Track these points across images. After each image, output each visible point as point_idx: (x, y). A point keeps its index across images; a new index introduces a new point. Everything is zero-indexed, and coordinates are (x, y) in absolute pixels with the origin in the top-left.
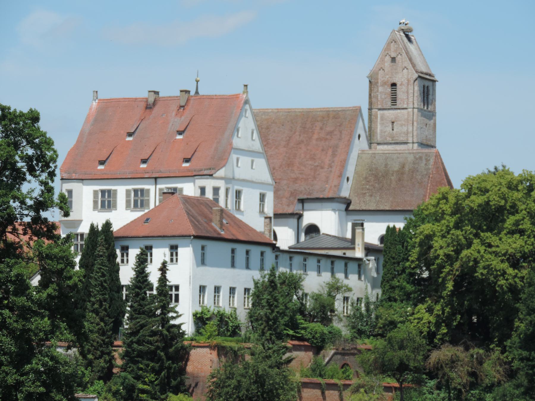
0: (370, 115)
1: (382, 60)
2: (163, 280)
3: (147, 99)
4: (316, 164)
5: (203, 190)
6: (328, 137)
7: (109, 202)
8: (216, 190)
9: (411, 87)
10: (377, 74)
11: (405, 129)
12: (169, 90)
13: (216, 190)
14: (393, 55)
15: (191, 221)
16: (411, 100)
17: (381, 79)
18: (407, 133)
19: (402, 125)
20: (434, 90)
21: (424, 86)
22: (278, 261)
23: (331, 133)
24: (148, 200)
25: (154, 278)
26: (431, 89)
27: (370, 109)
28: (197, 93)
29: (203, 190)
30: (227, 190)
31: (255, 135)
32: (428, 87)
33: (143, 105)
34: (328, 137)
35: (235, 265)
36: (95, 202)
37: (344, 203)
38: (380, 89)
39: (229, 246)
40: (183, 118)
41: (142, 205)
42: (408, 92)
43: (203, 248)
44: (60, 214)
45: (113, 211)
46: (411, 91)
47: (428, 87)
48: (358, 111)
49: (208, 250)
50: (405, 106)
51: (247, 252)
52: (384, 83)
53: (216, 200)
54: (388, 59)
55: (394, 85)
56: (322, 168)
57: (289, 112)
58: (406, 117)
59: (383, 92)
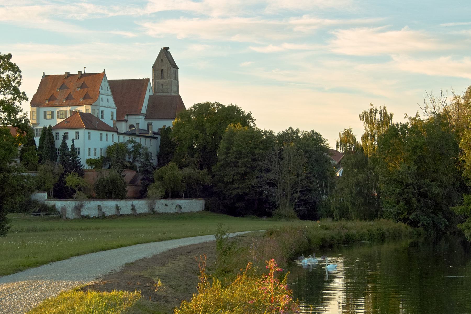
12: (74, 71)
14: (162, 58)
31: (109, 89)
55: (162, 70)
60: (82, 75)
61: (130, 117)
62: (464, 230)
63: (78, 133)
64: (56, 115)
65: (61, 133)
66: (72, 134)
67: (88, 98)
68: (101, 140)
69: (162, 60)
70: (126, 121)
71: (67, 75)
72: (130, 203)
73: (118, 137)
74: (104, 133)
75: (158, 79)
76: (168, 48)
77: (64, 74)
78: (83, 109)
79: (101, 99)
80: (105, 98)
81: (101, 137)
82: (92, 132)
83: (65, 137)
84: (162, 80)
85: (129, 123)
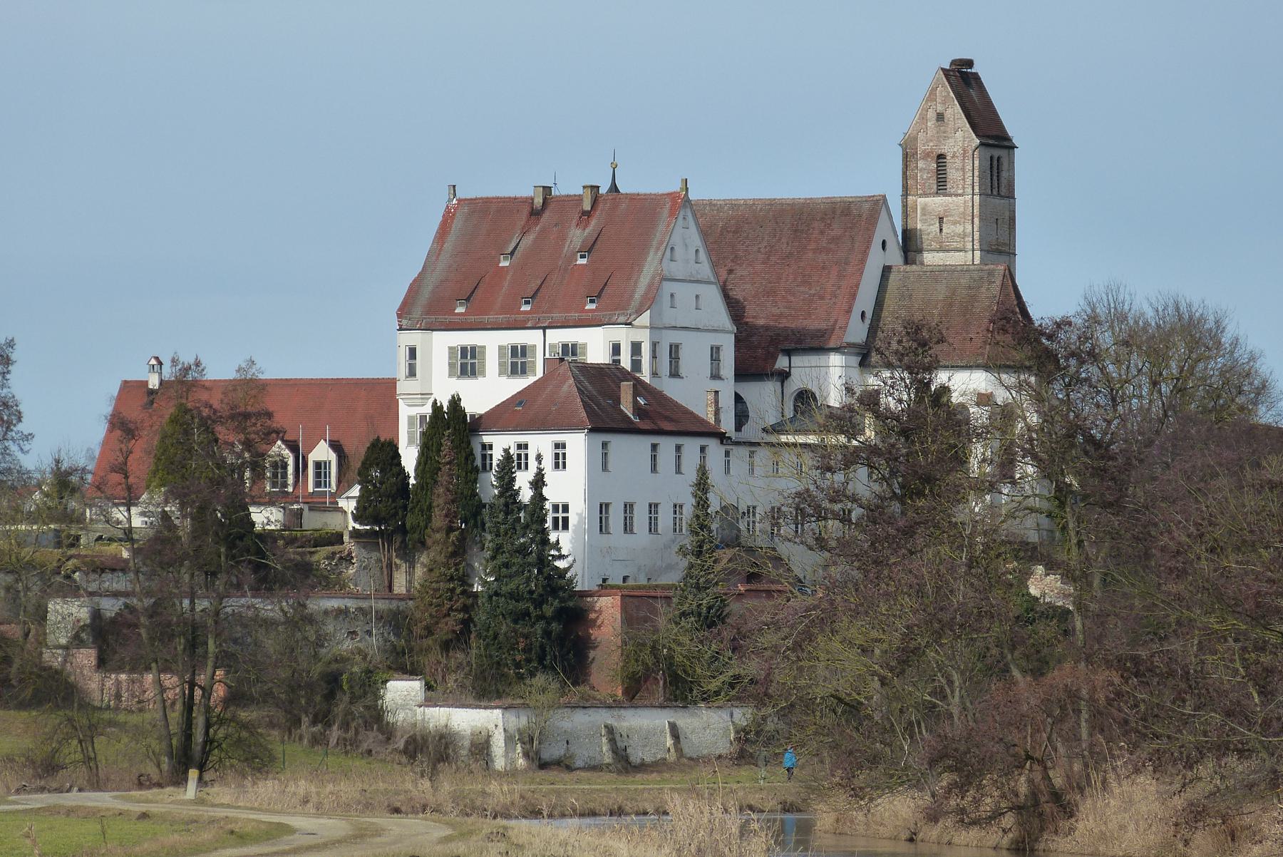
0: (905, 206)
1: (923, 118)
2: (539, 498)
3: (532, 199)
4: (813, 292)
5: (616, 349)
6: (832, 246)
7: (473, 365)
8: (636, 348)
9: (969, 162)
10: (916, 139)
11: (959, 229)
12: (569, 185)
13: (636, 348)
14: (940, 108)
15: (585, 405)
16: (969, 181)
17: (921, 148)
18: (965, 235)
19: (955, 223)
20: (1011, 163)
21: (992, 158)
22: (731, 458)
23: (835, 240)
24: (534, 363)
25: (526, 495)
26: (1005, 162)
27: (906, 193)
28: (614, 188)
29: (616, 349)
30: (654, 345)
31: (703, 256)
32: (999, 158)
33: (526, 210)
34: (832, 246)
35: (658, 468)
36: (451, 366)
37: (857, 354)
38: (921, 164)
39: (647, 441)
40: (587, 231)
41: (524, 372)
42: (963, 169)
43: (605, 445)
44: (497, 258)
45: (480, 379)
46: (969, 167)
47: (999, 158)
48: (879, 203)
49: (612, 449)
50: (960, 192)
51: (678, 448)
52: (927, 155)
53: (636, 365)
54: (931, 114)
55: (941, 156)
56: (822, 298)
57: (771, 203)
58: (962, 210)
59: (925, 168)
60: (601, 202)
61: (797, 360)
62: (138, 733)
63: (564, 446)
64: (492, 362)
65: (500, 443)
66: (540, 443)
67: (604, 298)
68: (654, 469)
69: (940, 117)
70: (784, 376)
71: (539, 201)
72: (603, 717)
73: (727, 454)
74: (667, 445)
75: (925, 195)
76: (970, 63)
77: (528, 192)
78: (596, 345)
79: (667, 298)
80: (685, 292)
81: (654, 458)
82: (620, 443)
83: (510, 464)
84: (939, 200)
85: (795, 384)
